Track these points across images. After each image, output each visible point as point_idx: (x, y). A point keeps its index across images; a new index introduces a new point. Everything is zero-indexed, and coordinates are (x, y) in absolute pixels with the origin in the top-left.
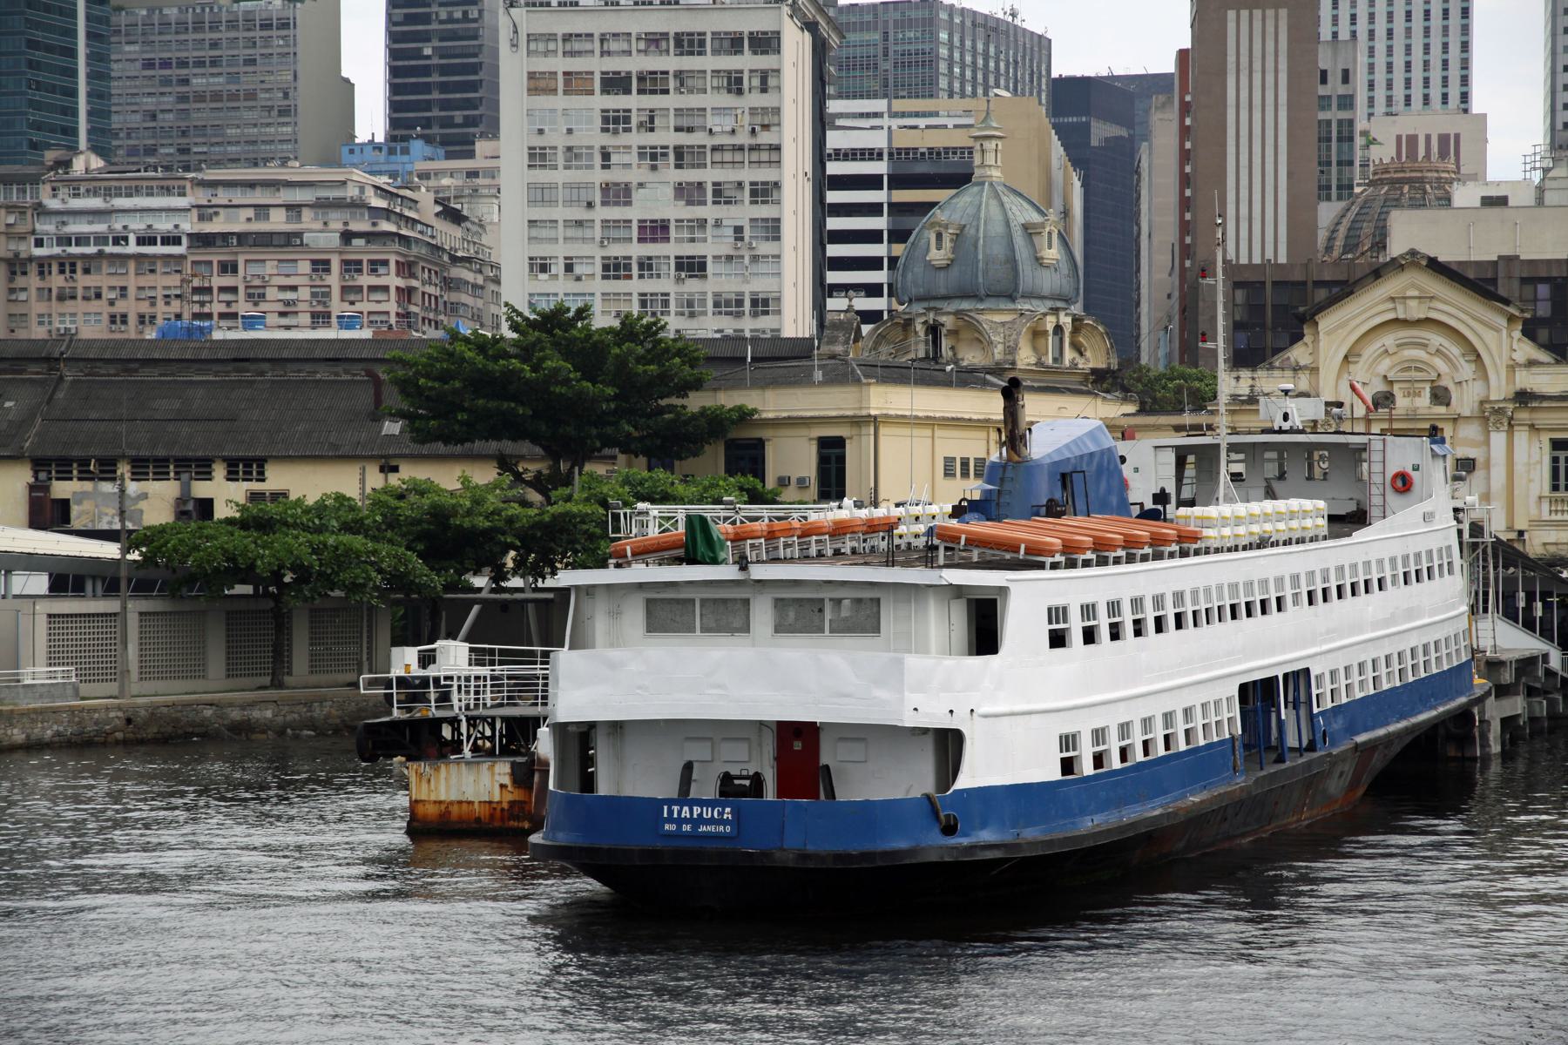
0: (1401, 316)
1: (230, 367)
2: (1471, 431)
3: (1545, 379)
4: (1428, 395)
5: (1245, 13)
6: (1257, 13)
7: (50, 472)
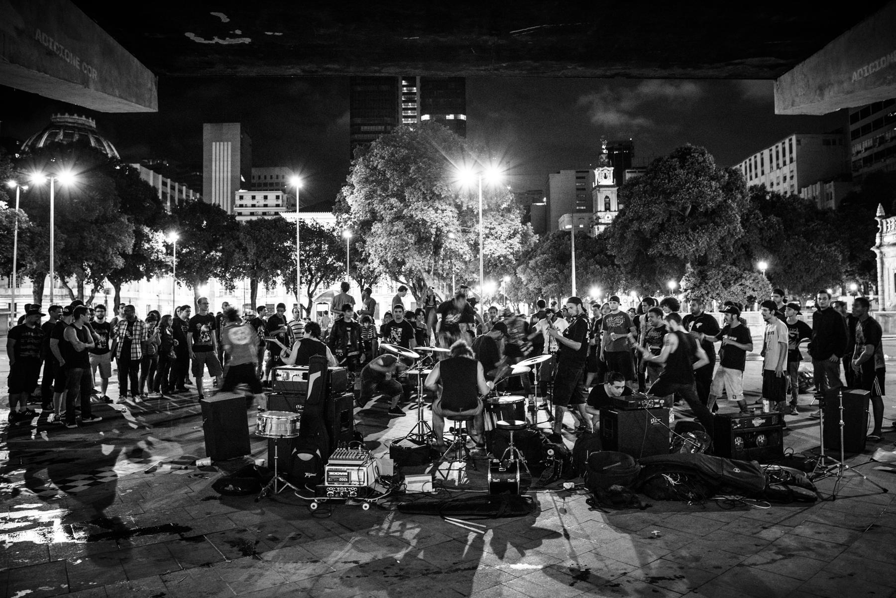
5: (218, 143)
6: (222, 143)
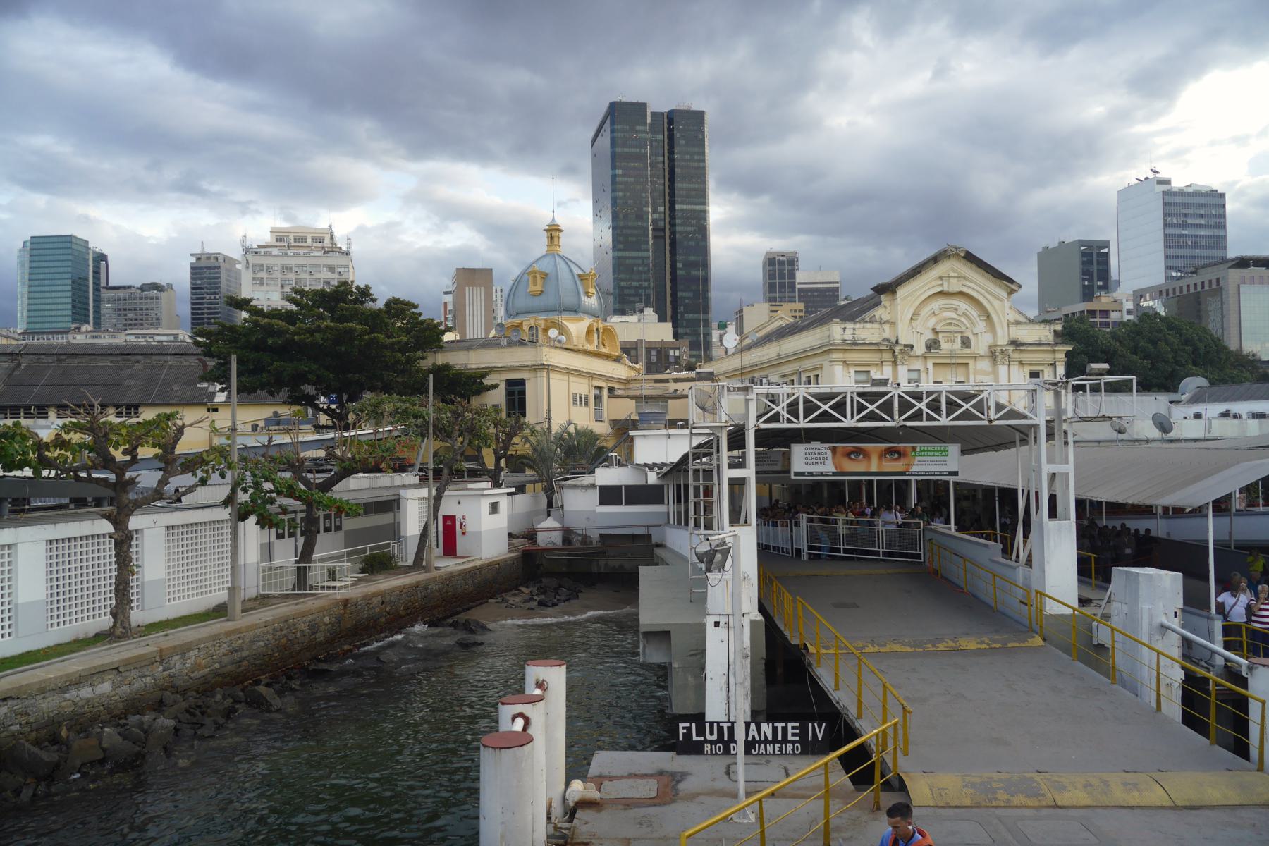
0: (946, 289)
1: (120, 358)
2: (984, 365)
3: (1025, 332)
4: (959, 341)
5: (471, 288)
7: (6, 414)
